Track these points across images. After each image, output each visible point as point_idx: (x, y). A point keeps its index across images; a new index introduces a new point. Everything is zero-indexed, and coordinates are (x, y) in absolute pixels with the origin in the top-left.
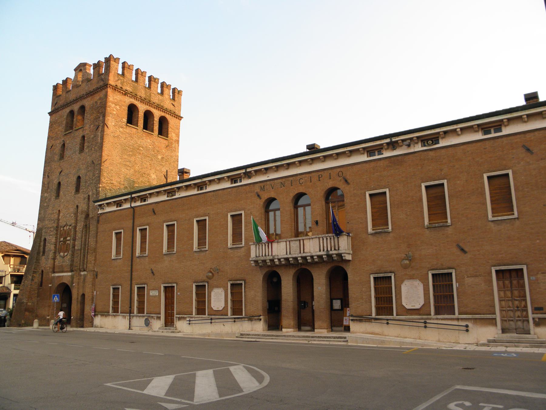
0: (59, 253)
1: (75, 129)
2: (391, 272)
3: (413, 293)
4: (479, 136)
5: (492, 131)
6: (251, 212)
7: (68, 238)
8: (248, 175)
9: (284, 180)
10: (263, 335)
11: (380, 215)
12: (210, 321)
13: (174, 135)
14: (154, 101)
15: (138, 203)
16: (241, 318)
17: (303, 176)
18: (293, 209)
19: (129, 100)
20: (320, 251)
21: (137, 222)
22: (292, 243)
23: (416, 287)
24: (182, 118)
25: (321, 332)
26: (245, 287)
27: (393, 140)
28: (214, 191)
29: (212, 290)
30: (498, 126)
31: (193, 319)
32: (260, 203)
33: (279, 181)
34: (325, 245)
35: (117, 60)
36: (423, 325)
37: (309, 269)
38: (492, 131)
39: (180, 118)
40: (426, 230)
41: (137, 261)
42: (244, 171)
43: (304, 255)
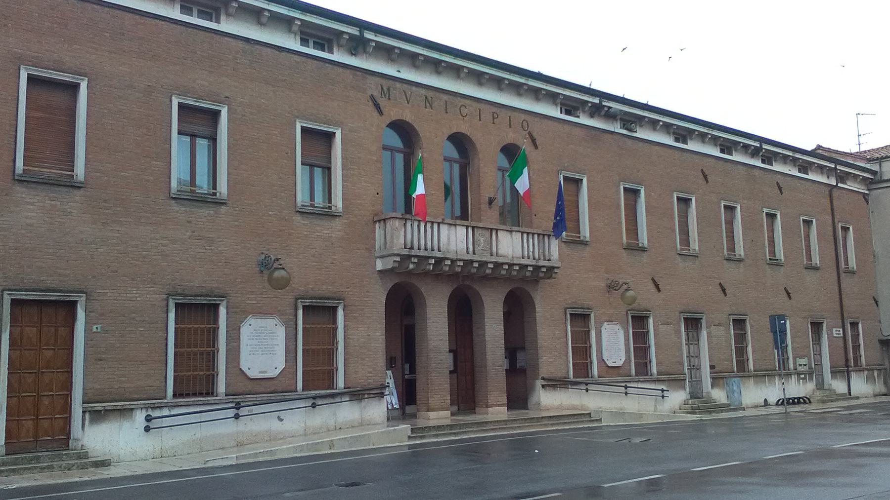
5: (195, 12)
8: (357, 45)
10: (451, 427)
12: (231, 413)
16: (333, 396)
20: (468, 253)
28: (247, 40)
30: (768, 158)
31: (165, 412)
33: (423, 91)
38: (195, 12)
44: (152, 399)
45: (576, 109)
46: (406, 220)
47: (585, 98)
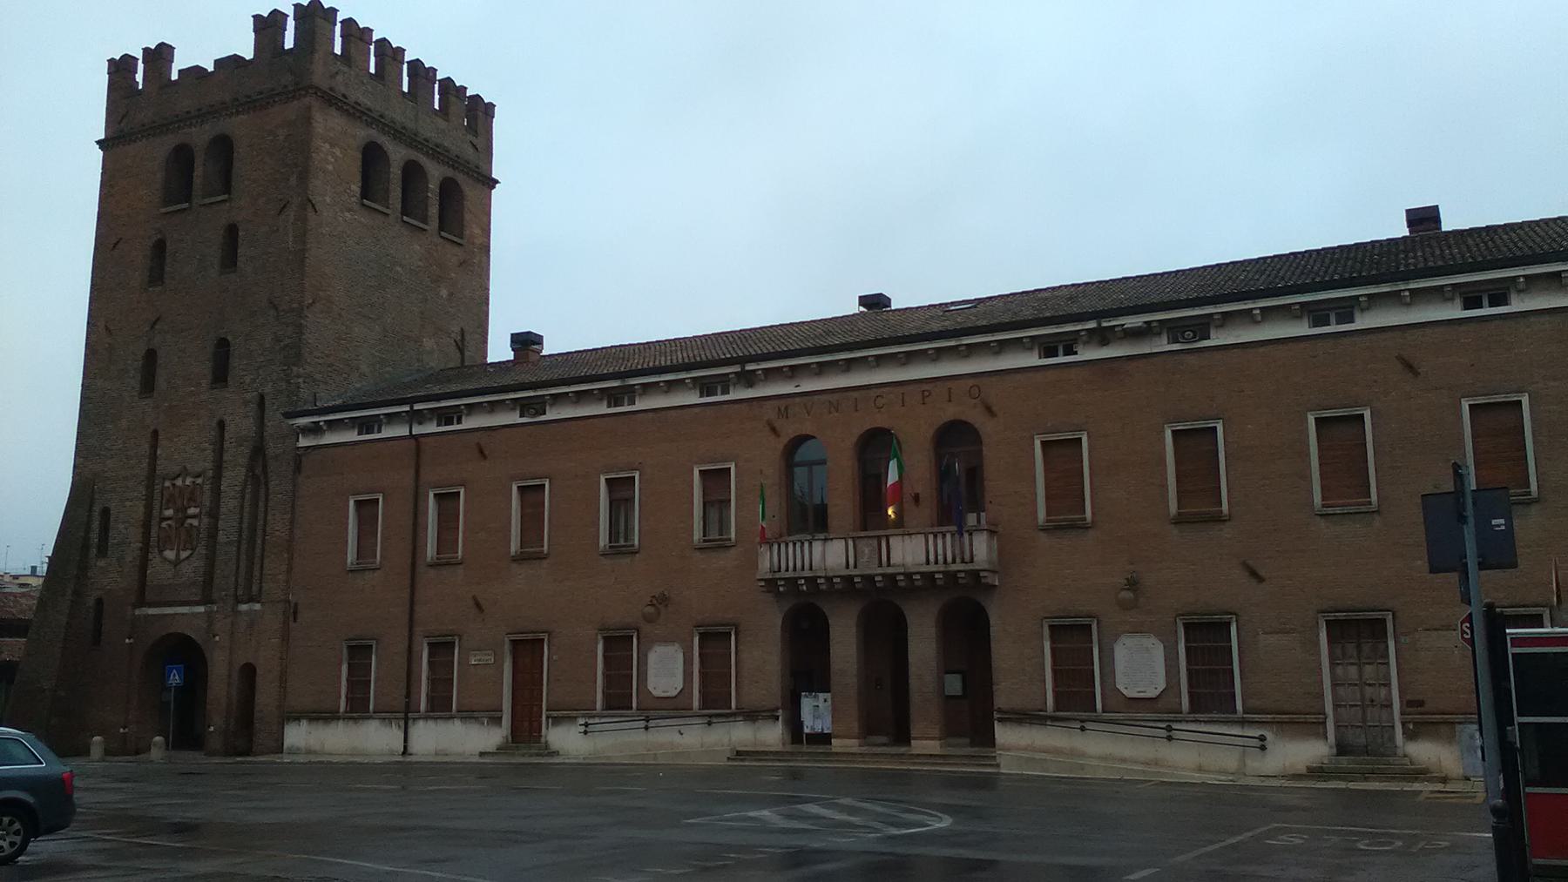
0: (161, 552)
3: (1140, 664)
4: (1302, 329)
5: (1333, 319)
6: (753, 464)
7: (192, 511)
11: (1065, 489)
12: (643, 724)
13: (477, 231)
15: (431, 428)
19: (363, 133)
22: (861, 544)
29: (650, 649)
34: (940, 551)
36: (1164, 733)
38: (1333, 319)
43: (890, 570)
44: (587, 709)
45: (1075, 341)
46: (879, 538)
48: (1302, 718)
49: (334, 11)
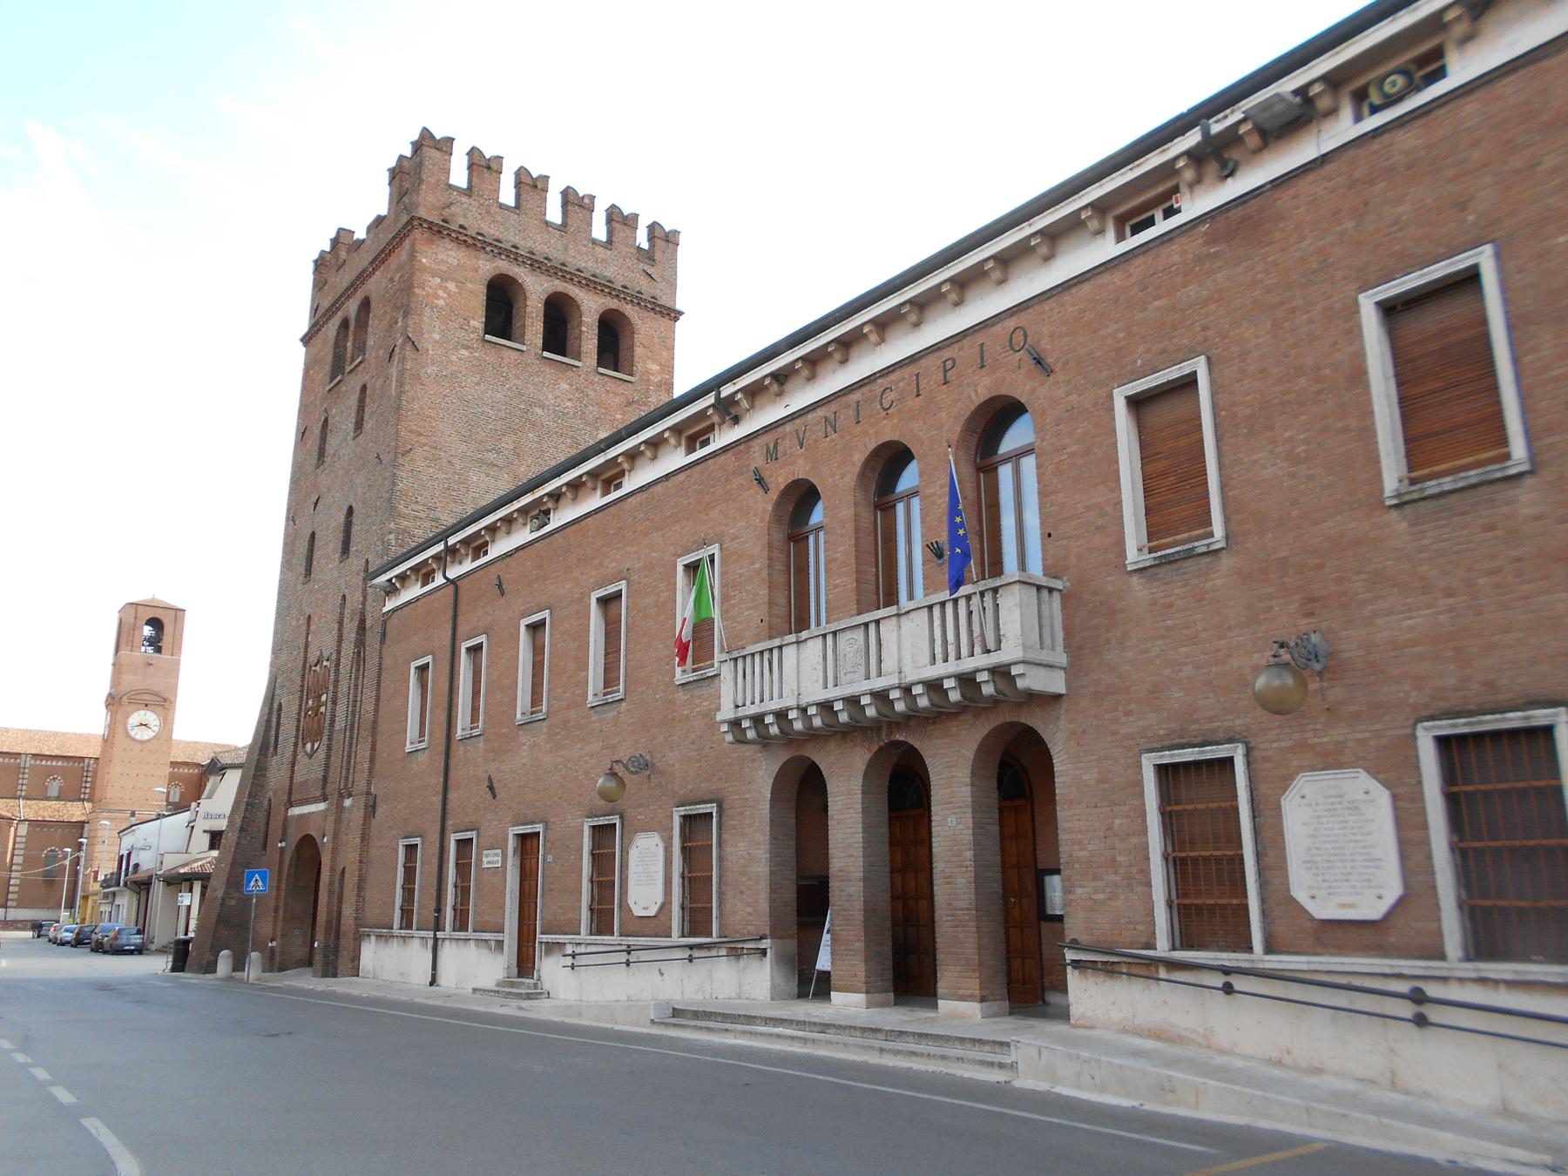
1: (348, 369)
2: (1230, 741)
8: (729, 411)
9: (833, 407)
12: (623, 957)
14: (582, 265)
16: (708, 946)
17: (893, 377)
18: (867, 515)
19: (488, 267)
21: (463, 629)
22: (843, 639)
23: (1354, 808)
24: (681, 313)
25: (960, 1010)
26: (720, 828)
27: (1216, 128)
28: (667, 477)
32: (763, 504)
33: (820, 413)
35: (446, 145)
36: (1406, 1009)
37: (917, 745)
39: (674, 315)
40: (1394, 514)
41: (458, 751)
42: (710, 400)
45: (1438, 53)
47: (1154, 160)
48: (1357, 982)
49: (635, 217)
